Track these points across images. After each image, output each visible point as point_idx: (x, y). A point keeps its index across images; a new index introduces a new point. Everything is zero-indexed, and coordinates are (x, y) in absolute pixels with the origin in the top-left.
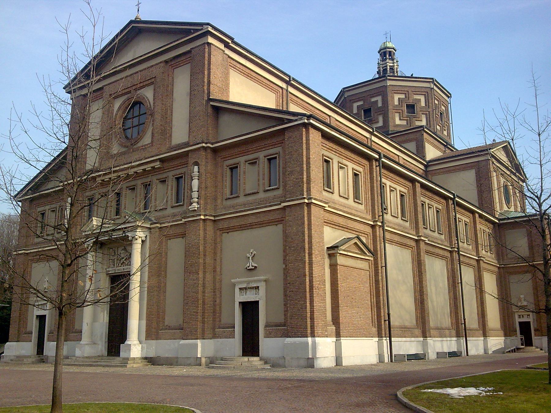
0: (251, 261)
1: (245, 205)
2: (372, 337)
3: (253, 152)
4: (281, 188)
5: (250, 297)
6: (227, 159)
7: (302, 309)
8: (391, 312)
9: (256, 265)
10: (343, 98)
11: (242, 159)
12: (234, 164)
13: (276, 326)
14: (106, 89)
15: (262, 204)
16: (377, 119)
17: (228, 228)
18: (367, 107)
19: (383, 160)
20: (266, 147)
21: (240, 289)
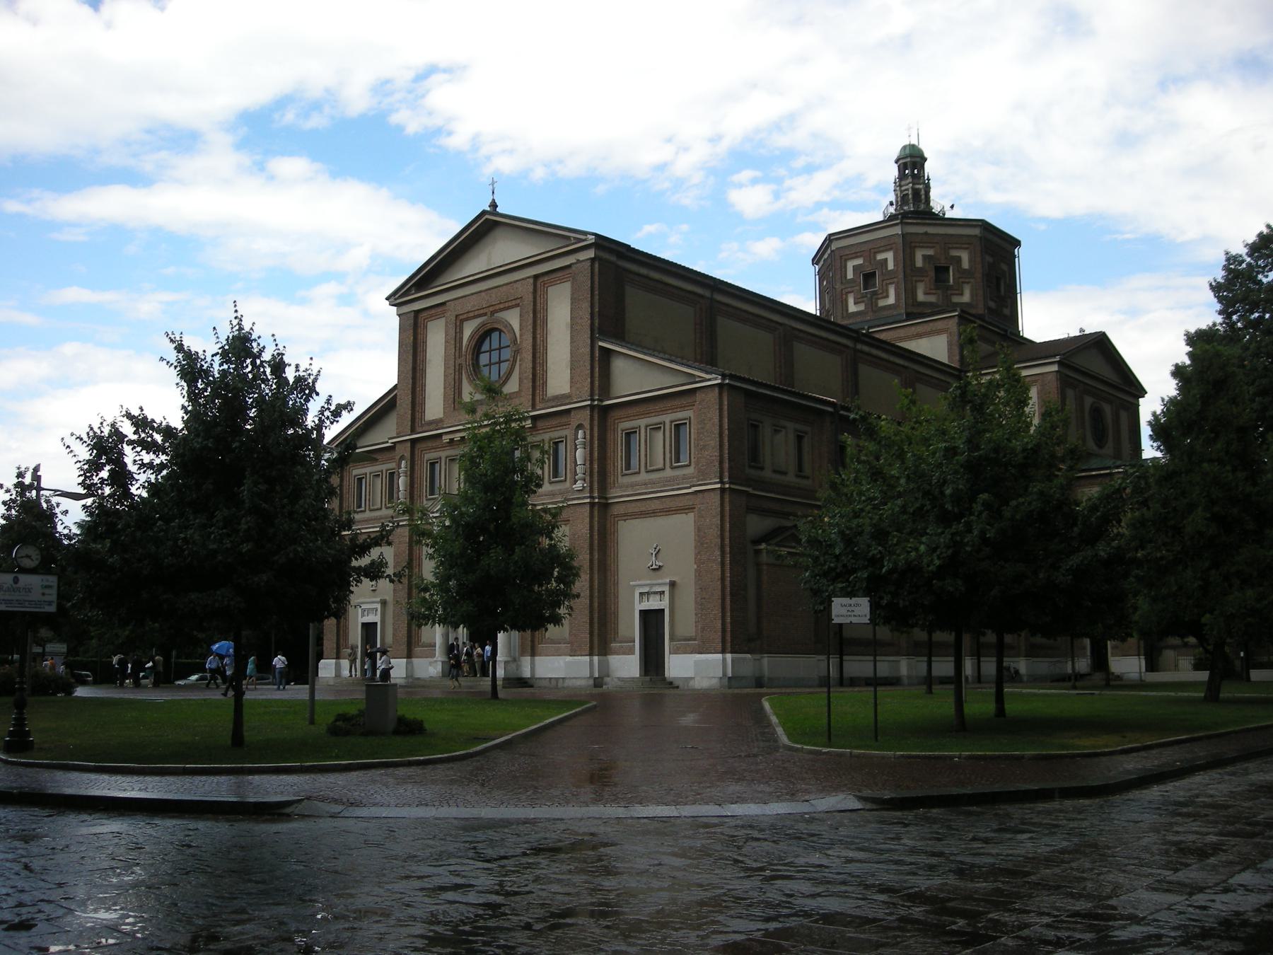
5: (653, 604)
11: (642, 422)
14: (450, 306)
16: (887, 291)
17: (625, 515)
18: (868, 270)
20: (674, 409)
21: (641, 594)
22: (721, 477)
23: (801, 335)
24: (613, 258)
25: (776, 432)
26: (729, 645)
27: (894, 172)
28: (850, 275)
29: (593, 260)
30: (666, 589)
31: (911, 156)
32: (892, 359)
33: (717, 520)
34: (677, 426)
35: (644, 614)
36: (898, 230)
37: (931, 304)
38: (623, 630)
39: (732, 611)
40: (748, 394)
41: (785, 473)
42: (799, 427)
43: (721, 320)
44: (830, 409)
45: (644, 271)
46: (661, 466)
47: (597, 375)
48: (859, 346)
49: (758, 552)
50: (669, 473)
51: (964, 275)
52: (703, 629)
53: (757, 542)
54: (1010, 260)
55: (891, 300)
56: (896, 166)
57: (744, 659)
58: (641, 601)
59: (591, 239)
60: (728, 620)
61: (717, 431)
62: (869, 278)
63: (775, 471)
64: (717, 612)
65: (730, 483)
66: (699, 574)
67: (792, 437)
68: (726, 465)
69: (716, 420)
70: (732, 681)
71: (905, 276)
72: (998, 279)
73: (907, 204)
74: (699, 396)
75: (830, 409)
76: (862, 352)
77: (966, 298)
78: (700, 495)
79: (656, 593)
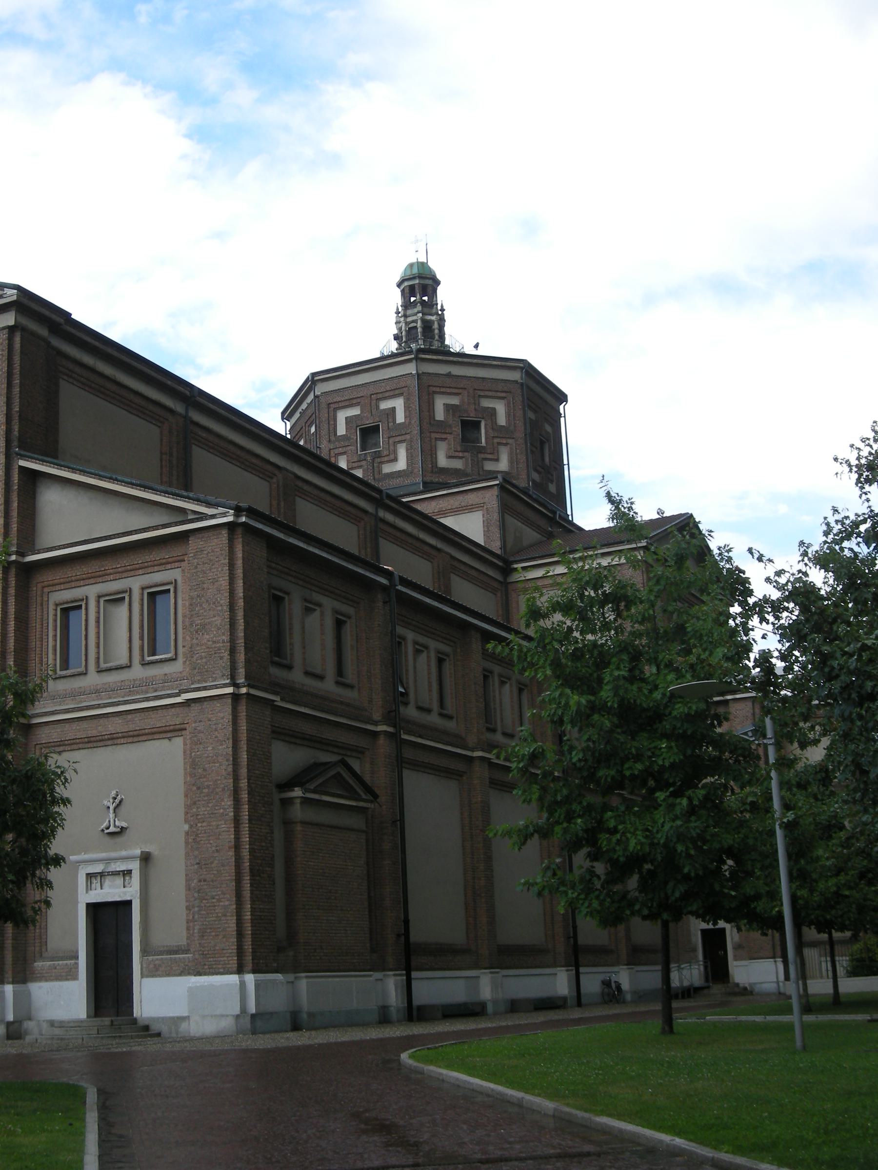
0: (112, 815)
1: (97, 691)
2: (370, 970)
3: (118, 576)
4: (181, 659)
6: (57, 588)
7: (225, 916)
8: (411, 917)
9: (124, 824)
10: (311, 397)
11: (92, 591)
12: (72, 602)
13: (170, 952)
15: (138, 693)
16: (395, 452)
17: (61, 743)
18: (369, 422)
19: (399, 587)
20: (145, 568)
21: (90, 876)
22: (233, 677)
23: (306, 487)
24: (44, 332)
25: (308, 611)
26: (249, 958)
27: (396, 298)
28: (341, 430)
29: (11, 329)
30: (135, 866)
31: (420, 277)
32: (422, 535)
33: (226, 748)
34: (152, 596)
35: (94, 909)
36: (411, 368)
37: (456, 472)
38: (55, 937)
39: (253, 901)
40: (272, 543)
41: (321, 678)
42: (337, 605)
43: (198, 453)
44: (384, 581)
45: (88, 359)
46: (124, 661)
47: (15, 513)
48: (382, 513)
49: (286, 803)
50: (138, 672)
51: (502, 434)
52: (203, 934)
53: (286, 785)
54: (554, 419)
55: (401, 464)
56: (398, 292)
57: (274, 981)
58: (89, 888)
59: (11, 295)
60: (248, 916)
61: (225, 601)
62: (369, 433)
63: (307, 673)
64: (228, 902)
65: (249, 686)
66: (193, 839)
67: (329, 622)
68: (241, 657)
69: (224, 582)
70: (258, 1022)
71: (421, 432)
72: (542, 443)
73: (415, 340)
74: (194, 543)
75: (384, 581)
76: (383, 521)
77: (503, 465)
78: (195, 707)
79: (116, 873)
